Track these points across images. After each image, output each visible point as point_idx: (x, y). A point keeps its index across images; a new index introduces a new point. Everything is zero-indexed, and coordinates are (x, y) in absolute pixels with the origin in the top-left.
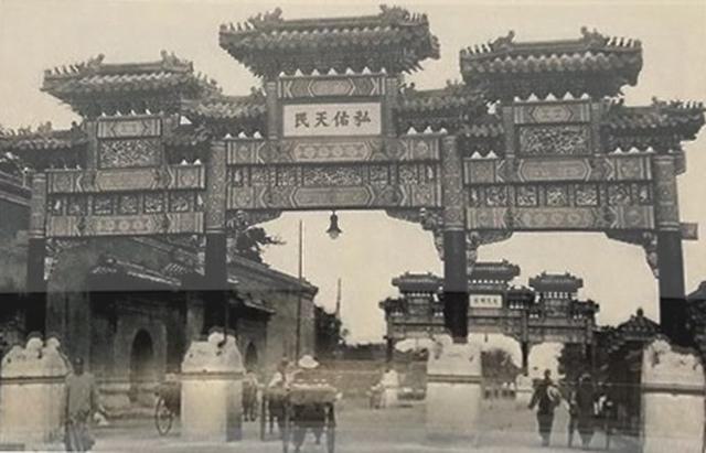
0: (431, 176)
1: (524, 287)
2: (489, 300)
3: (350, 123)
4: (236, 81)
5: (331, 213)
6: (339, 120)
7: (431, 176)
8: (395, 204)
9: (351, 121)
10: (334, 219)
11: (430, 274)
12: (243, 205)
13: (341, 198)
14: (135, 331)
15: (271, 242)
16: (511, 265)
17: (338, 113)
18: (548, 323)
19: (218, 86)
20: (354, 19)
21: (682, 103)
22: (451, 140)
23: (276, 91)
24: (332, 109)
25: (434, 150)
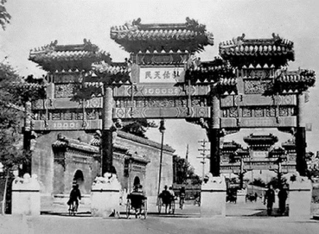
1: (280, 148)
2: (262, 153)
3: (171, 77)
11: (271, 135)
14: (75, 171)
15: (149, 126)
16: (273, 137)
19: (111, 57)
20: (174, 25)
21: (308, 71)
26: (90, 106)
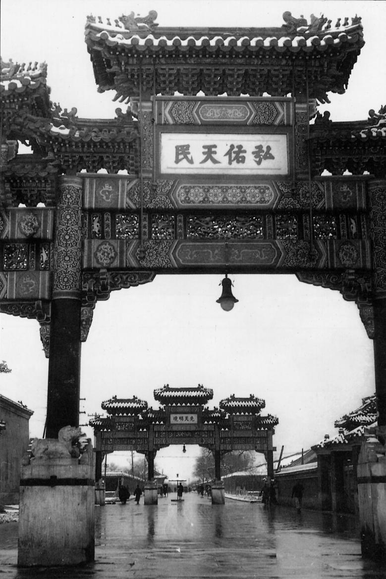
0: (354, 231)
5: (223, 276)
6: (233, 155)
7: (354, 231)
8: (311, 265)
9: (250, 159)
10: (227, 284)
12: (105, 262)
13: (237, 259)
17: (232, 146)
18: (236, 434)
23: (152, 113)
25: (360, 196)
26: (13, 233)
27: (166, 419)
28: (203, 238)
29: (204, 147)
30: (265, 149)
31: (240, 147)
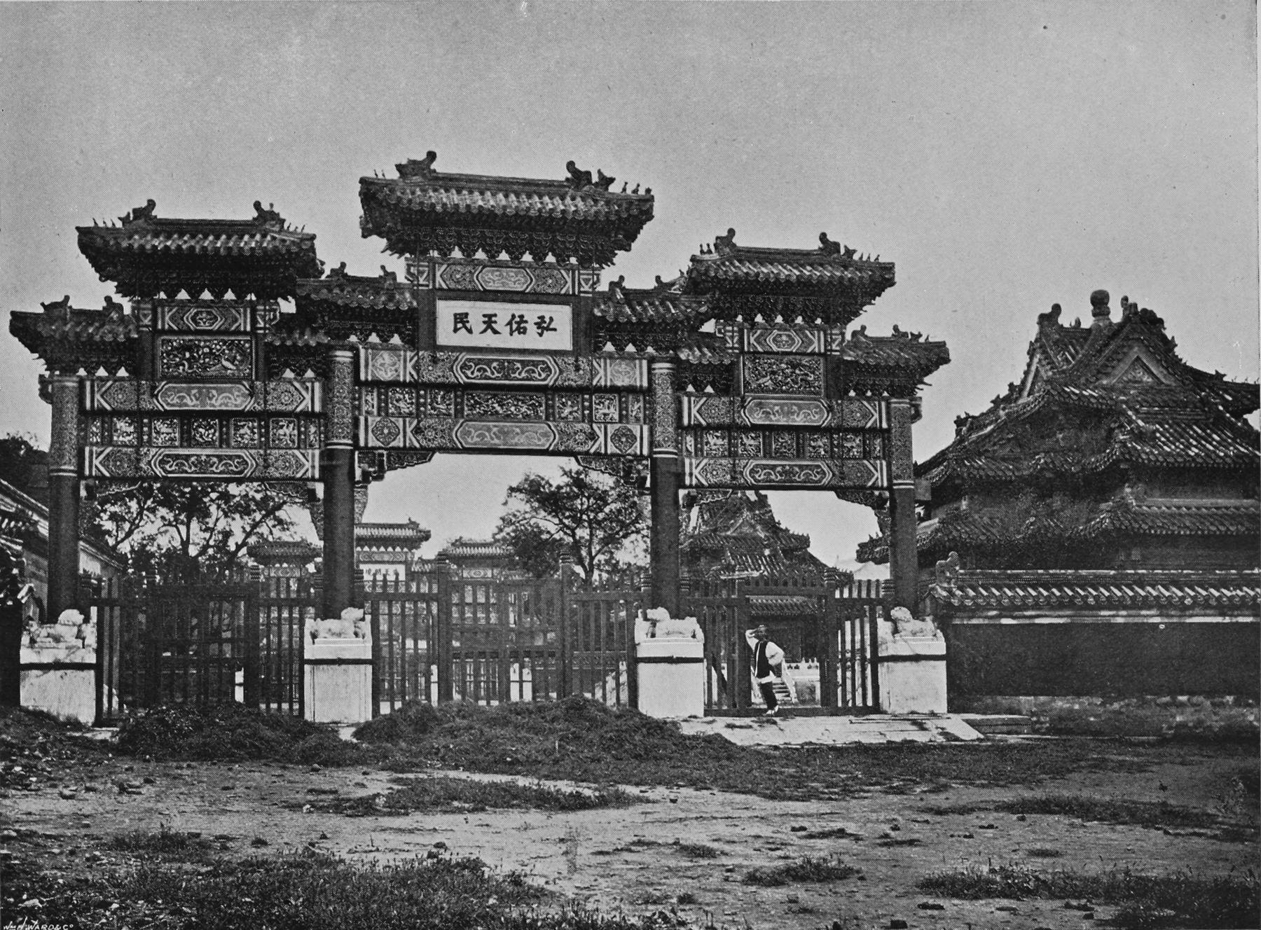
4: (352, 251)
6: (515, 326)
9: (532, 329)
17: (513, 316)
22: (662, 368)
24: (503, 312)
27: (413, 326)
28: (482, 417)
29: (484, 316)
30: (547, 320)
31: (521, 317)
